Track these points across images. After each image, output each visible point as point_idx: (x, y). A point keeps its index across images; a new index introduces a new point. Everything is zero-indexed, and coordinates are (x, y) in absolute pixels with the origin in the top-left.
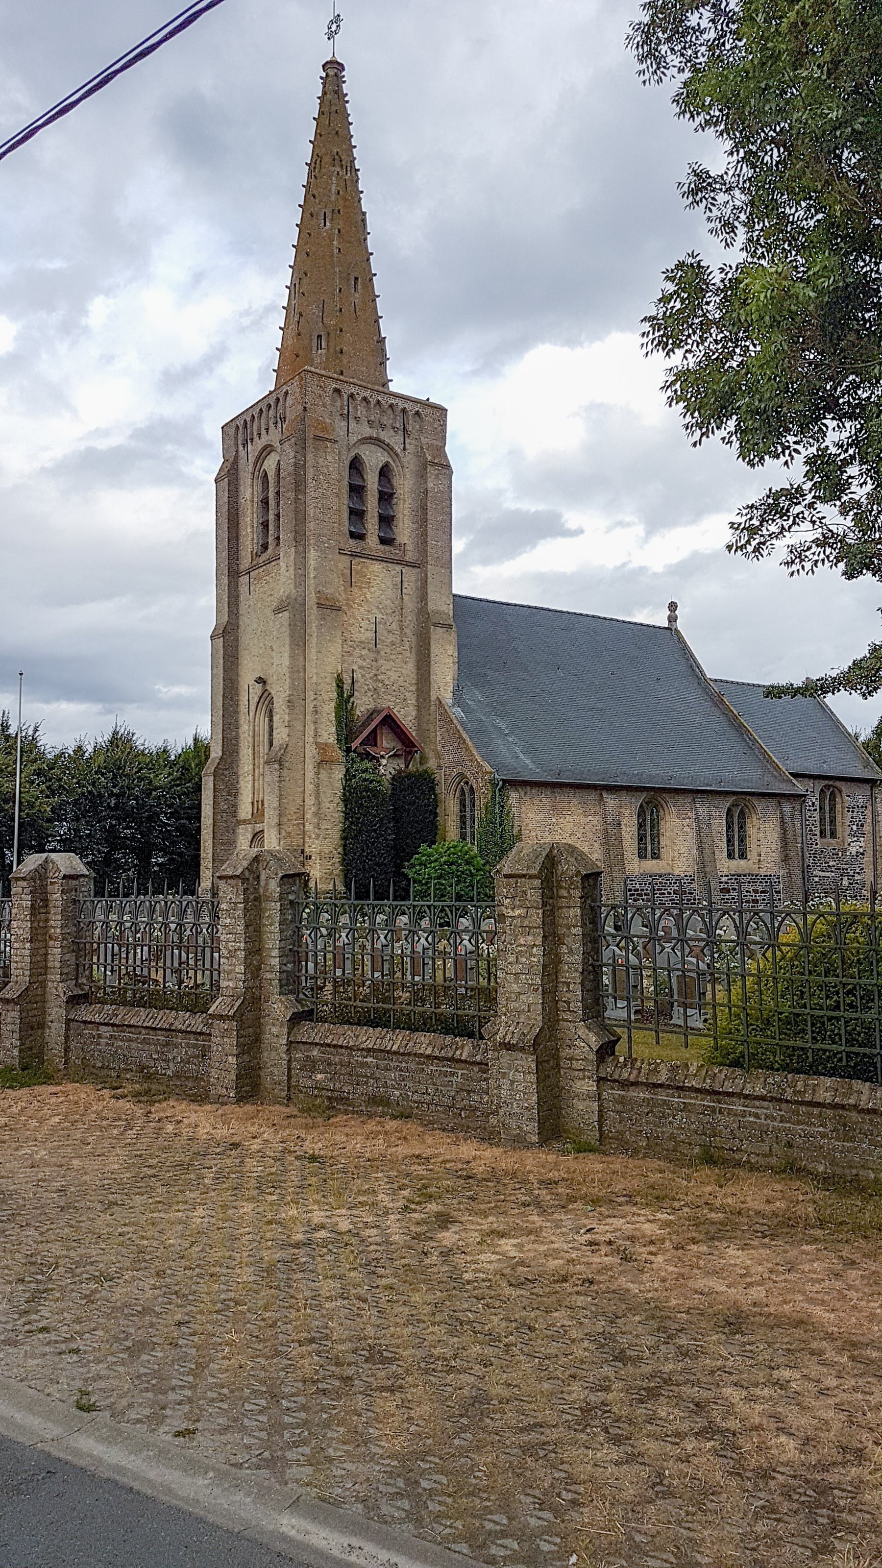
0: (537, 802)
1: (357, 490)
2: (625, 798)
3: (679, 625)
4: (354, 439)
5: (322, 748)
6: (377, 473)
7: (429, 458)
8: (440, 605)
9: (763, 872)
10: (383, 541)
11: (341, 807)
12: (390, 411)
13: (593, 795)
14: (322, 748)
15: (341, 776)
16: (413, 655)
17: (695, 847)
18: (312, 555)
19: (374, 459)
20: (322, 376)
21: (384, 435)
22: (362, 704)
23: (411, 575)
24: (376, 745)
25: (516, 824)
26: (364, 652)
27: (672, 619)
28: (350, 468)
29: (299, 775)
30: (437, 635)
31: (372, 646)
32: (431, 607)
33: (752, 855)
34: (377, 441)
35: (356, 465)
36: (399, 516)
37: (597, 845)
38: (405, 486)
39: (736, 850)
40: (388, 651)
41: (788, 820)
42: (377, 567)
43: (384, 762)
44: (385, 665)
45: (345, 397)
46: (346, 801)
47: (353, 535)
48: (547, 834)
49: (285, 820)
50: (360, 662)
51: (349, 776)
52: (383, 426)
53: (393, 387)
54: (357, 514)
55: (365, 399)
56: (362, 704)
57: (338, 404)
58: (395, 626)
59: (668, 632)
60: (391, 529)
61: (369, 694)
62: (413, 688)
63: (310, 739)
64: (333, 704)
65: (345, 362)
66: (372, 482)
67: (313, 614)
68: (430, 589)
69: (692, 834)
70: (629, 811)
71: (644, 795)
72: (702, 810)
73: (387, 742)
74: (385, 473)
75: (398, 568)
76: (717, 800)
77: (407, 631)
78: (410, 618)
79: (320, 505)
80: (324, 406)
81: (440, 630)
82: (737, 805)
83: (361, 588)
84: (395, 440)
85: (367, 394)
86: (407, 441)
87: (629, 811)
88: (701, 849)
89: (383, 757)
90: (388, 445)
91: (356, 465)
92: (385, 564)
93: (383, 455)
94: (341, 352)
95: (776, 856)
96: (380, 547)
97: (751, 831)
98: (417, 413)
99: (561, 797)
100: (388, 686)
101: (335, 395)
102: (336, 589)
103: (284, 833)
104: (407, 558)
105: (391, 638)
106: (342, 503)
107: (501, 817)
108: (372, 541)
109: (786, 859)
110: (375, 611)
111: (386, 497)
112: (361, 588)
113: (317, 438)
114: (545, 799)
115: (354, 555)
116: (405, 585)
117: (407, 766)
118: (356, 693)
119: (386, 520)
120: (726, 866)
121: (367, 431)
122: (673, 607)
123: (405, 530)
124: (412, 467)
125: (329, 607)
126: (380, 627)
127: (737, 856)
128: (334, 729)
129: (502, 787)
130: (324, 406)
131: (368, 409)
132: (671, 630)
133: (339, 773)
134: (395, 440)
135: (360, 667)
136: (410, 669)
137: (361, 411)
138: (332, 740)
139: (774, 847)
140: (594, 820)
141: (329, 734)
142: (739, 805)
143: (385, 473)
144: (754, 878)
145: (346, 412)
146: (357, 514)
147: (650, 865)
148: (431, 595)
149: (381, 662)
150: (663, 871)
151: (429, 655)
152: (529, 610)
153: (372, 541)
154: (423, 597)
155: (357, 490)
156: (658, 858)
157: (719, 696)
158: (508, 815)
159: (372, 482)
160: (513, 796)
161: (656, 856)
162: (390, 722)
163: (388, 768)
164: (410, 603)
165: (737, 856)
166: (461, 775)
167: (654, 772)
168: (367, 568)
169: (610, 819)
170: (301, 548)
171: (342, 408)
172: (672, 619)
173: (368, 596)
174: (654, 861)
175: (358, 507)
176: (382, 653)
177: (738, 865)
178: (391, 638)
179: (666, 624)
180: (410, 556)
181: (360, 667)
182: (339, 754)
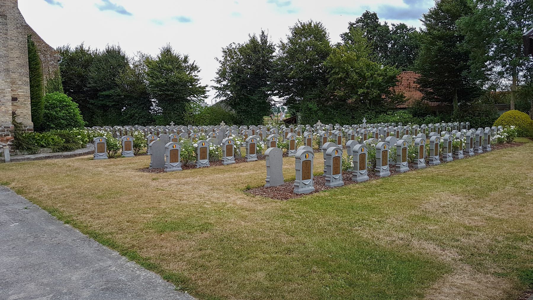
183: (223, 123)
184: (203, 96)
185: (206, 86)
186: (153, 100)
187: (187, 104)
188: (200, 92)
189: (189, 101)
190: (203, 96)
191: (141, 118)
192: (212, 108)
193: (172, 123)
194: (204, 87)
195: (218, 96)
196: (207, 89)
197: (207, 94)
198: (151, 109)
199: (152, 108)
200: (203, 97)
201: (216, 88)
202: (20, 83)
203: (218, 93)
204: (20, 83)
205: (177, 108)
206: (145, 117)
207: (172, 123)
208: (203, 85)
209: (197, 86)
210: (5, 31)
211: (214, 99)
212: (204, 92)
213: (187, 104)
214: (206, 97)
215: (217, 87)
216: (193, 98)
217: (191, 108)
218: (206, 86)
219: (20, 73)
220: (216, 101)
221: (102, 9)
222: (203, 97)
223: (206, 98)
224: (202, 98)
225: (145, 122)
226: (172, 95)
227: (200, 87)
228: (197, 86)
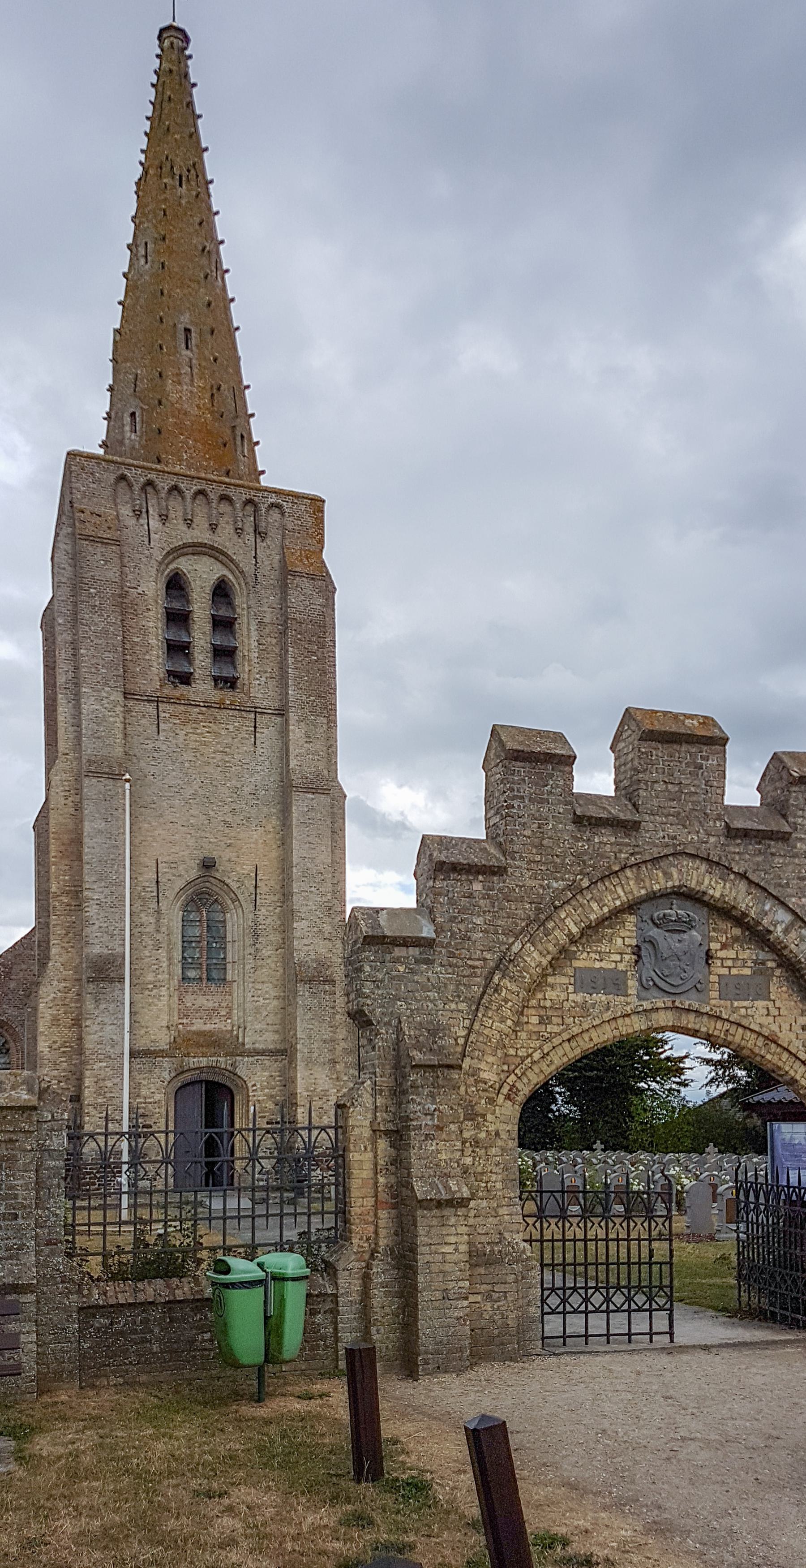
19: (202, 575)
35: (176, 585)
53: (264, 481)
91: (176, 585)
134: (239, 549)
143: (221, 592)
159: (201, 609)
183: (711, 1148)
184: (677, 1080)
185: (686, 1057)
186: (557, 1089)
187: (635, 1100)
188: (669, 1070)
189: (642, 1091)
190: (677, 1080)
191: (530, 1132)
192: (698, 1110)
193: (598, 1145)
194: (681, 1059)
195: (712, 1081)
196: (688, 1063)
197: (688, 1075)
198: (552, 1111)
199: (554, 1107)
200: (677, 1083)
201: (708, 1062)
202: (346, 1078)
203: (713, 1074)
204: (346, 1078)
205: (613, 1109)
206: (537, 1130)
207: (598, 1145)
208: (676, 1054)
209: (663, 1056)
210: (332, 1004)
211: (704, 1090)
212: (680, 1071)
213: (635, 1100)
214: (684, 1084)
215: (712, 1060)
216: (654, 1085)
217: (645, 1110)
218: (686, 1057)
219: (346, 1063)
220: (708, 1093)
221: (151, 102)
222: (677, 1083)
223: (686, 1085)
224: (674, 1086)
225: (539, 1143)
226: (600, 1079)
227: (668, 1059)
228: (663, 1056)
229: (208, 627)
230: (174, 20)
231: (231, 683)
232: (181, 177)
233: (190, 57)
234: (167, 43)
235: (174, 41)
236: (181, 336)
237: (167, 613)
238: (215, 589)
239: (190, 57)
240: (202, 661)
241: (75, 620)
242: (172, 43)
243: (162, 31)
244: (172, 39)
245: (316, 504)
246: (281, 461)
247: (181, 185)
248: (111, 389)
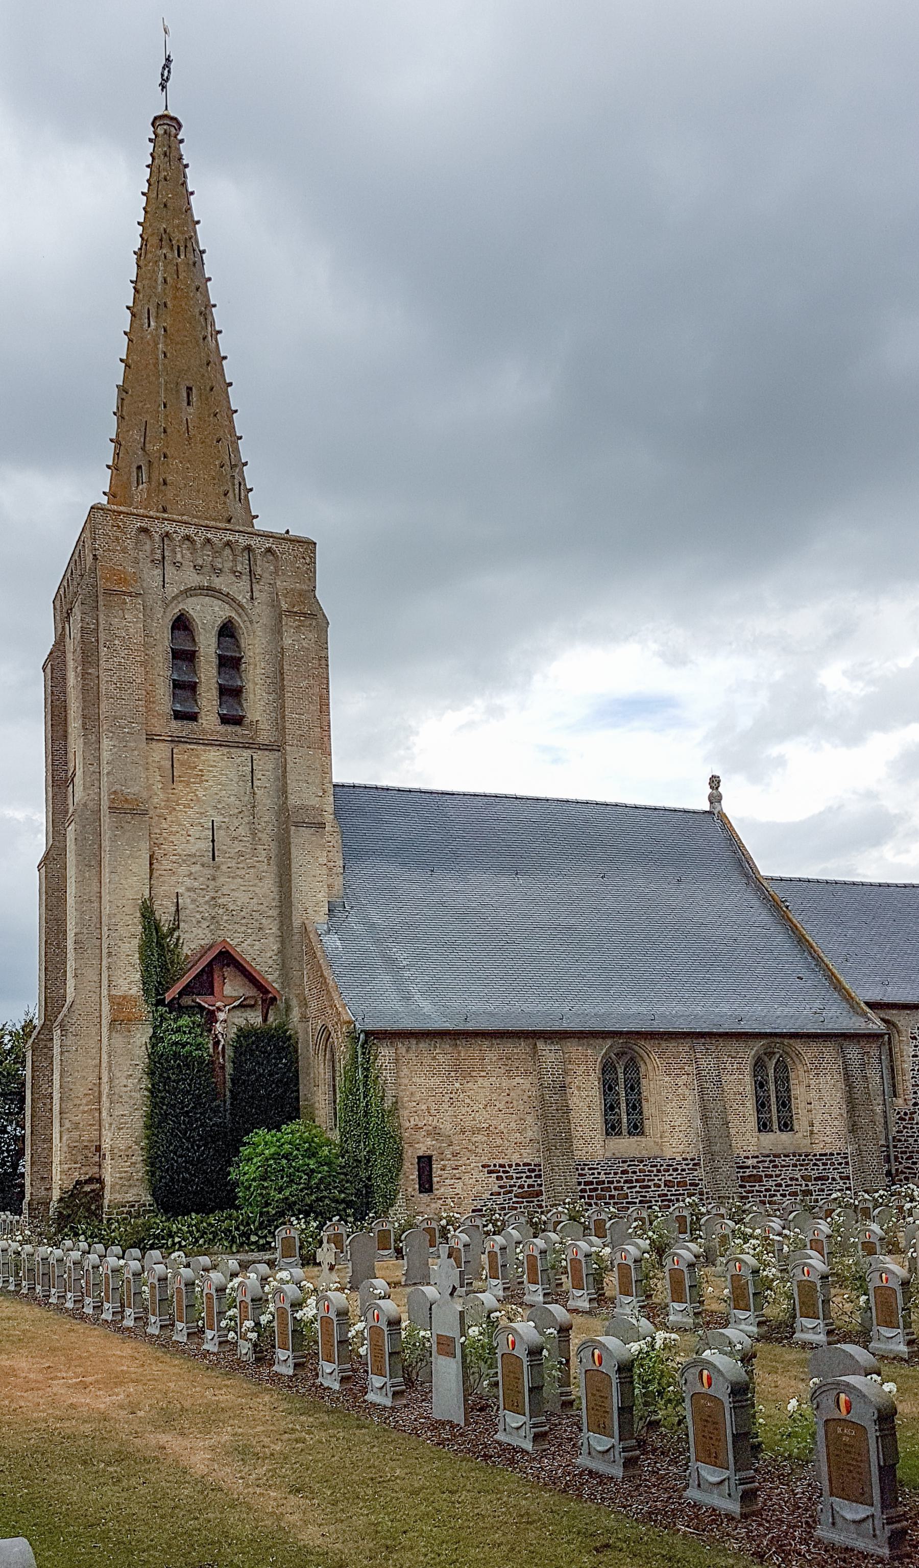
0: (428, 1060)
1: (184, 657)
2: (574, 1049)
3: (728, 807)
4: (172, 590)
5: (118, 1003)
6: (215, 632)
7: (285, 606)
8: (303, 794)
9: (818, 1149)
10: (225, 720)
11: (146, 1083)
12: (227, 551)
13: (521, 1048)
14: (118, 1003)
15: (145, 1039)
16: (274, 868)
17: (699, 1115)
18: (106, 743)
19: (207, 615)
20: (121, 513)
21: (218, 582)
22: (193, 940)
23: (265, 762)
24: (212, 994)
25: (389, 1093)
26: (195, 868)
27: (715, 799)
28: (173, 628)
29: (92, 1043)
30: (301, 838)
31: (207, 859)
32: (293, 800)
33: (801, 1124)
34: (210, 591)
35: (182, 624)
36: (249, 686)
37: (530, 1119)
38: (255, 646)
39: (775, 1118)
40: (233, 864)
41: (856, 1072)
42: (213, 754)
43: (221, 1016)
44: (227, 884)
45: (157, 537)
46: (151, 1074)
47: (178, 716)
48: (445, 1106)
49: (70, 1105)
50: (188, 882)
51: (156, 1039)
52: (218, 572)
53: (258, 525)
54: (185, 688)
55: (187, 538)
56: (193, 940)
57: (148, 547)
58: (242, 831)
59: (709, 818)
60: (241, 705)
61: (205, 924)
62: (274, 913)
63: (105, 992)
64: (136, 942)
65: (170, 495)
66: (207, 646)
67: (107, 820)
68: (291, 777)
69: (692, 1097)
70: (583, 1067)
71: (609, 1042)
72: (707, 1063)
73: (232, 988)
74: (227, 631)
75: (247, 753)
76: (734, 1046)
77: (264, 836)
78: (267, 818)
79: (115, 679)
80: (124, 550)
81: (305, 832)
82: (771, 1055)
83: (188, 783)
84: (239, 589)
85: (191, 531)
86: (256, 587)
87: (583, 1067)
88: (705, 1118)
89: (219, 1009)
90: (227, 595)
91: (182, 624)
92: (225, 750)
93: (223, 610)
94: (165, 483)
95: (839, 1125)
96: (219, 728)
97: (797, 1090)
98: (269, 550)
99: (469, 1052)
100: (224, 910)
101: (142, 536)
102: (146, 783)
103: (68, 1125)
104: (259, 740)
105: (238, 847)
106: (162, 673)
107: (365, 1084)
108: (209, 719)
109: (853, 1128)
110: (211, 812)
111: (230, 663)
112: (188, 783)
113: (109, 593)
114: (443, 1054)
115: (176, 741)
116: (258, 774)
117: (265, 1020)
118: (182, 925)
119: (231, 693)
120: (748, 1140)
121: (194, 579)
122: (715, 782)
123: (257, 705)
124: (264, 620)
125: (129, 809)
126: (220, 835)
127: (775, 1126)
128: (138, 976)
129: (366, 1042)
130: (124, 550)
131: (194, 551)
132: (714, 816)
133: (142, 1036)
134: (239, 589)
135: (189, 890)
136: (268, 887)
137: (183, 554)
138: (136, 990)
139: (836, 1112)
140: (525, 1083)
141: (129, 982)
142: (773, 1056)
143: (227, 631)
144: (802, 1158)
145: (158, 556)
146: (185, 688)
147: (626, 1145)
148: (292, 786)
149: (222, 880)
150: (645, 1153)
151: (290, 865)
152: (486, 800)
153: (209, 719)
154: (283, 791)
155: (184, 657)
156: (642, 1133)
157: (778, 901)
158: (375, 1081)
159: (207, 646)
160: (385, 1053)
161: (637, 1129)
162: (226, 959)
163: (229, 1024)
164: (266, 800)
165: (775, 1126)
166: (325, 1028)
167: (626, 1011)
168: (198, 756)
169: (548, 1080)
170: (93, 738)
171: (153, 551)
172: (715, 799)
173: (200, 794)
174: (634, 1139)
175: (186, 678)
176: (224, 867)
177: (776, 1140)
178: (238, 847)
179: (707, 807)
180: (264, 737)
181: (189, 890)
182: (144, 1009)
229: (215, 693)
230: (166, 109)
231: (237, 721)
232: (179, 247)
233: (182, 141)
234: (160, 131)
235: (166, 128)
236: (410, 1172)
237: (179, 618)
238: (221, 628)
239: (182, 141)
240: (208, 702)
241: (89, 656)
242: (165, 131)
243: (156, 118)
244: (165, 127)
245: (310, 545)
246: (276, 506)
247: (179, 256)
248: (117, 442)
